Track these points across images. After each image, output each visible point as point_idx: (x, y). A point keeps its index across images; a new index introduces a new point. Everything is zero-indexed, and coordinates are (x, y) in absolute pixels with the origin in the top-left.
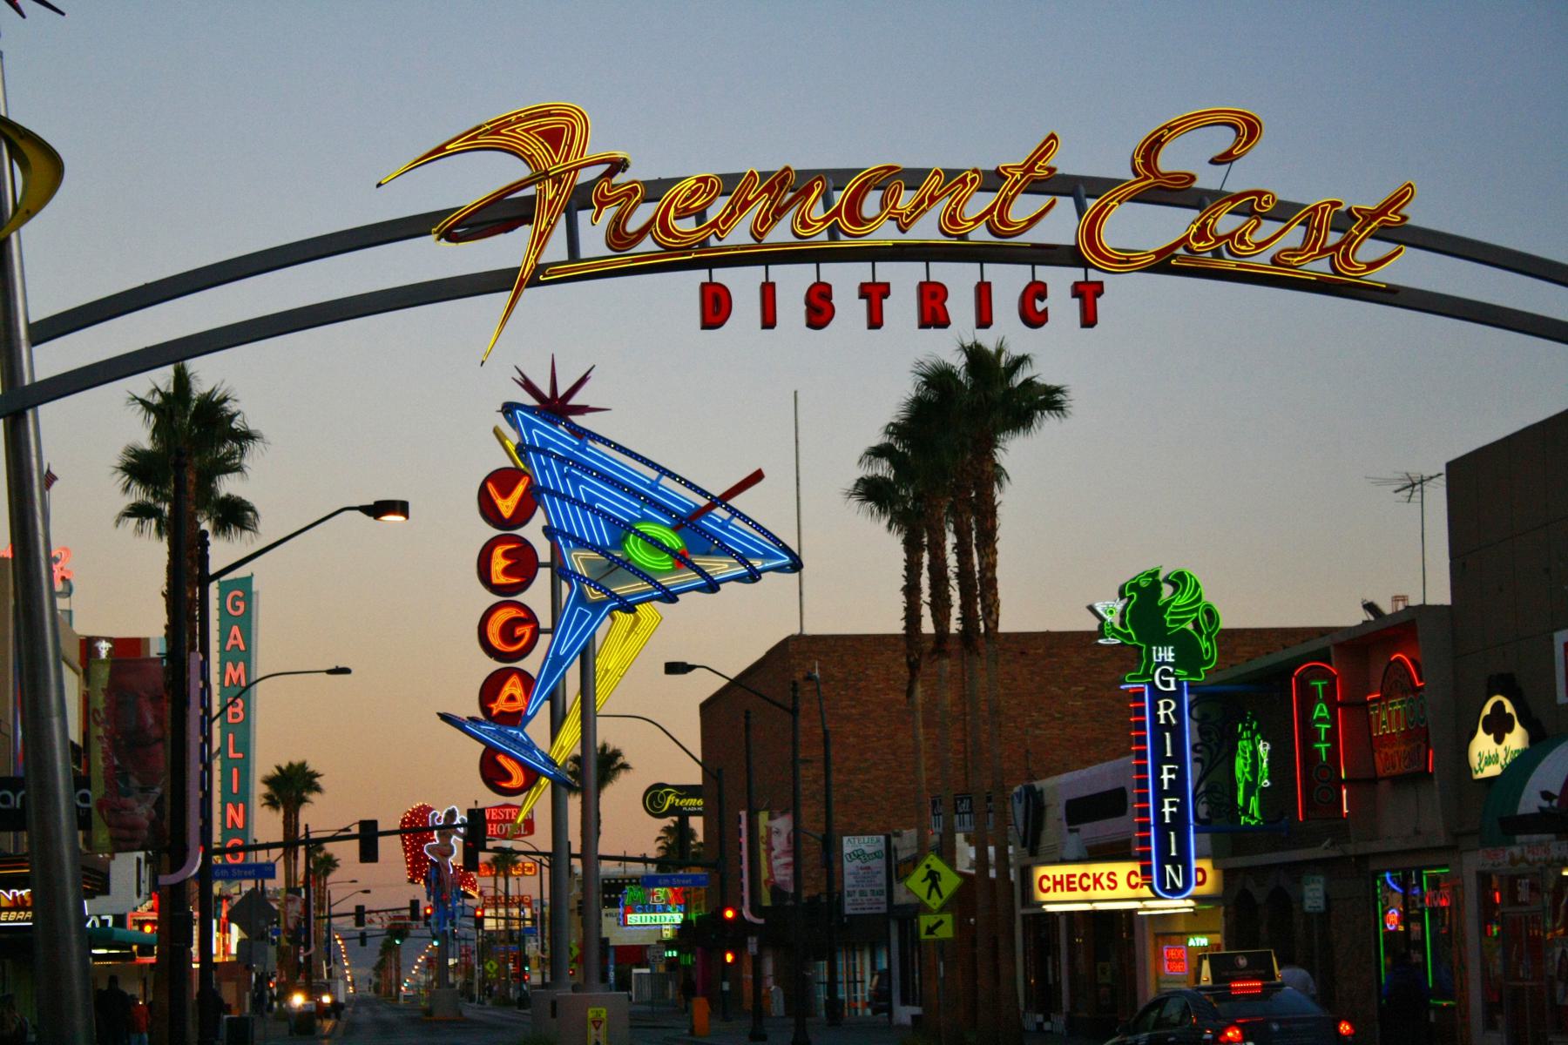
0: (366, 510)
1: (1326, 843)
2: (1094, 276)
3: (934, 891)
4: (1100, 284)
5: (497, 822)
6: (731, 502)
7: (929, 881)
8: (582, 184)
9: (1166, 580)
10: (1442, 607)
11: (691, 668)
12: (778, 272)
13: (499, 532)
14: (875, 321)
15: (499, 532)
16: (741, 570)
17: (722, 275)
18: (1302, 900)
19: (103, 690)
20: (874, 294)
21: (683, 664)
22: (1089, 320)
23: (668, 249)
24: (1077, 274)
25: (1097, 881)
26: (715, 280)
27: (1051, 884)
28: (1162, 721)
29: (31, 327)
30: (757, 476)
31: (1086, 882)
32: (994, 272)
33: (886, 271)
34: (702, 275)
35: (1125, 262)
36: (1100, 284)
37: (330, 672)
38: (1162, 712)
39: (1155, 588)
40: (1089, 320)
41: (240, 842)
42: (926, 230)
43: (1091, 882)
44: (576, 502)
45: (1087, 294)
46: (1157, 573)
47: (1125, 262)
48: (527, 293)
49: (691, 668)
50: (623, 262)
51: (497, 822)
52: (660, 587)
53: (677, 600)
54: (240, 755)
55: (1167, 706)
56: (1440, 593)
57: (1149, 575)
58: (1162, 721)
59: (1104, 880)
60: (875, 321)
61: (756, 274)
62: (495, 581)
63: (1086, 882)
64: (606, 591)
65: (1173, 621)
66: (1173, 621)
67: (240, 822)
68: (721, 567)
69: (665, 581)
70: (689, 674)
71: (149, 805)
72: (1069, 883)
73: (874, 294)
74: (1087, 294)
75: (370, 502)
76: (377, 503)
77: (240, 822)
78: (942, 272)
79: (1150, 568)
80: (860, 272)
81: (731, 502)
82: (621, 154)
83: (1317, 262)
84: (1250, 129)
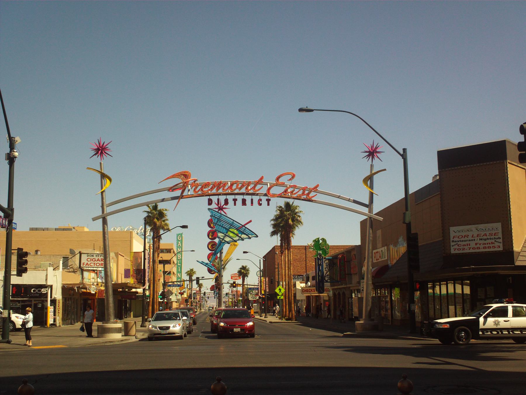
0: (180, 227)
1: (344, 285)
2: (269, 198)
3: (280, 292)
4: (270, 199)
5: (234, 277)
6: (245, 226)
7: (279, 290)
8: (108, 213)
9: (321, 240)
10: (359, 245)
11: (247, 252)
12: (220, 197)
13: (211, 229)
14: (235, 204)
15: (211, 229)
16: (248, 237)
17: (211, 197)
18: (186, 297)
19: (132, 257)
20: (235, 200)
21: (246, 252)
22: (268, 204)
23: (203, 193)
24: (267, 198)
25: (312, 290)
26: (210, 198)
27: (304, 291)
28: (319, 264)
29: (106, 205)
30: (250, 221)
31: (310, 290)
32: (254, 197)
33: (237, 197)
34: (208, 197)
35: (274, 196)
36: (270, 199)
37: (191, 251)
38: (319, 262)
39: (319, 241)
40: (268, 204)
41: (180, 280)
42: (243, 190)
43: (311, 291)
44: (220, 226)
45: (268, 200)
46: (319, 238)
47: (274, 196)
48: (181, 200)
49: (247, 252)
50: (196, 194)
51: (234, 277)
52: (233, 240)
53: (244, 240)
54: (180, 265)
55: (320, 261)
56: (360, 244)
57: (317, 239)
58: (319, 264)
59: (313, 290)
60: (235, 204)
61: (217, 197)
62: (210, 238)
63: (310, 290)
64: (233, 239)
65: (321, 246)
66: (321, 246)
67: (180, 276)
68: (243, 236)
69: (235, 239)
70: (247, 253)
71: (140, 276)
72: (307, 291)
73: (235, 200)
74: (268, 200)
75: (182, 226)
76: (183, 226)
77: (180, 276)
78: (246, 197)
79: (318, 237)
80: (233, 197)
81: (245, 226)
82: (196, 179)
83: (66, 254)
84: (294, 176)
